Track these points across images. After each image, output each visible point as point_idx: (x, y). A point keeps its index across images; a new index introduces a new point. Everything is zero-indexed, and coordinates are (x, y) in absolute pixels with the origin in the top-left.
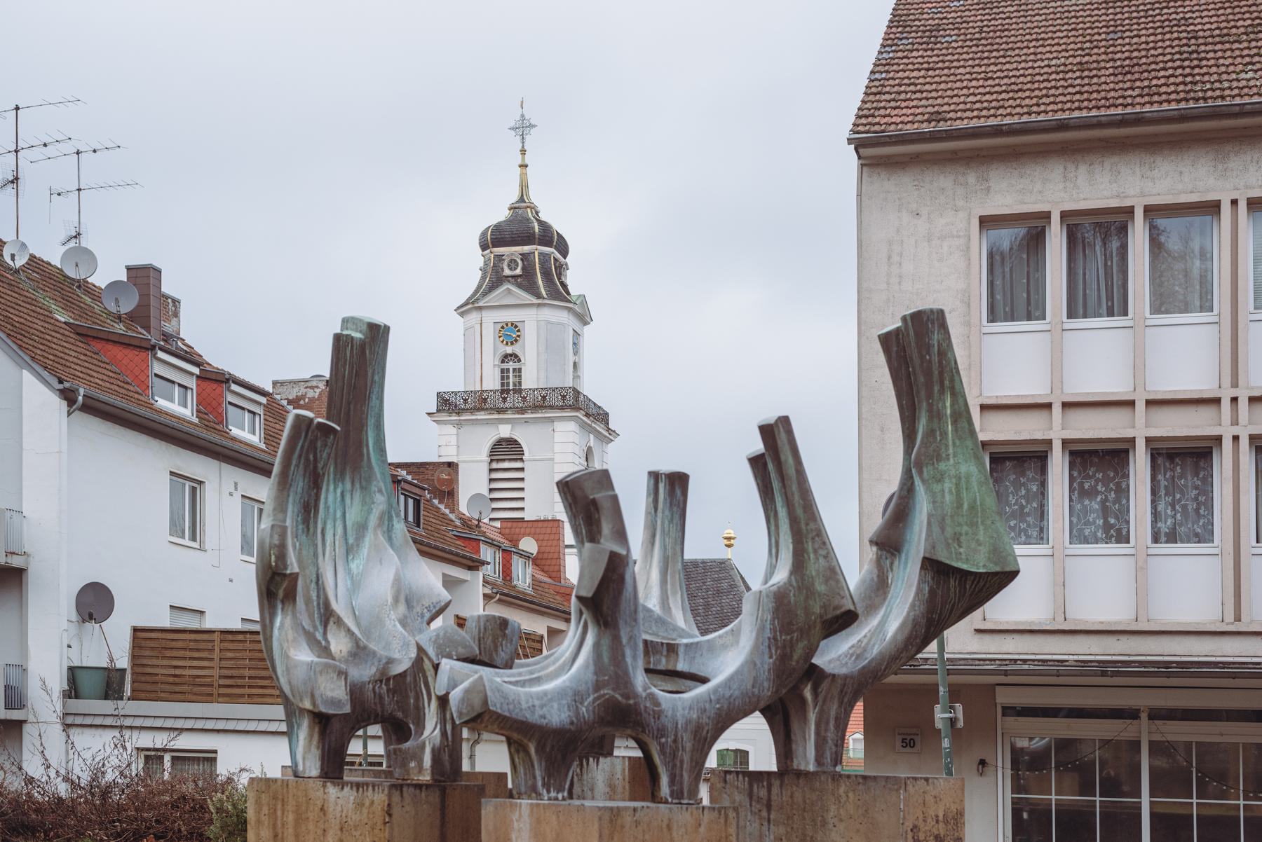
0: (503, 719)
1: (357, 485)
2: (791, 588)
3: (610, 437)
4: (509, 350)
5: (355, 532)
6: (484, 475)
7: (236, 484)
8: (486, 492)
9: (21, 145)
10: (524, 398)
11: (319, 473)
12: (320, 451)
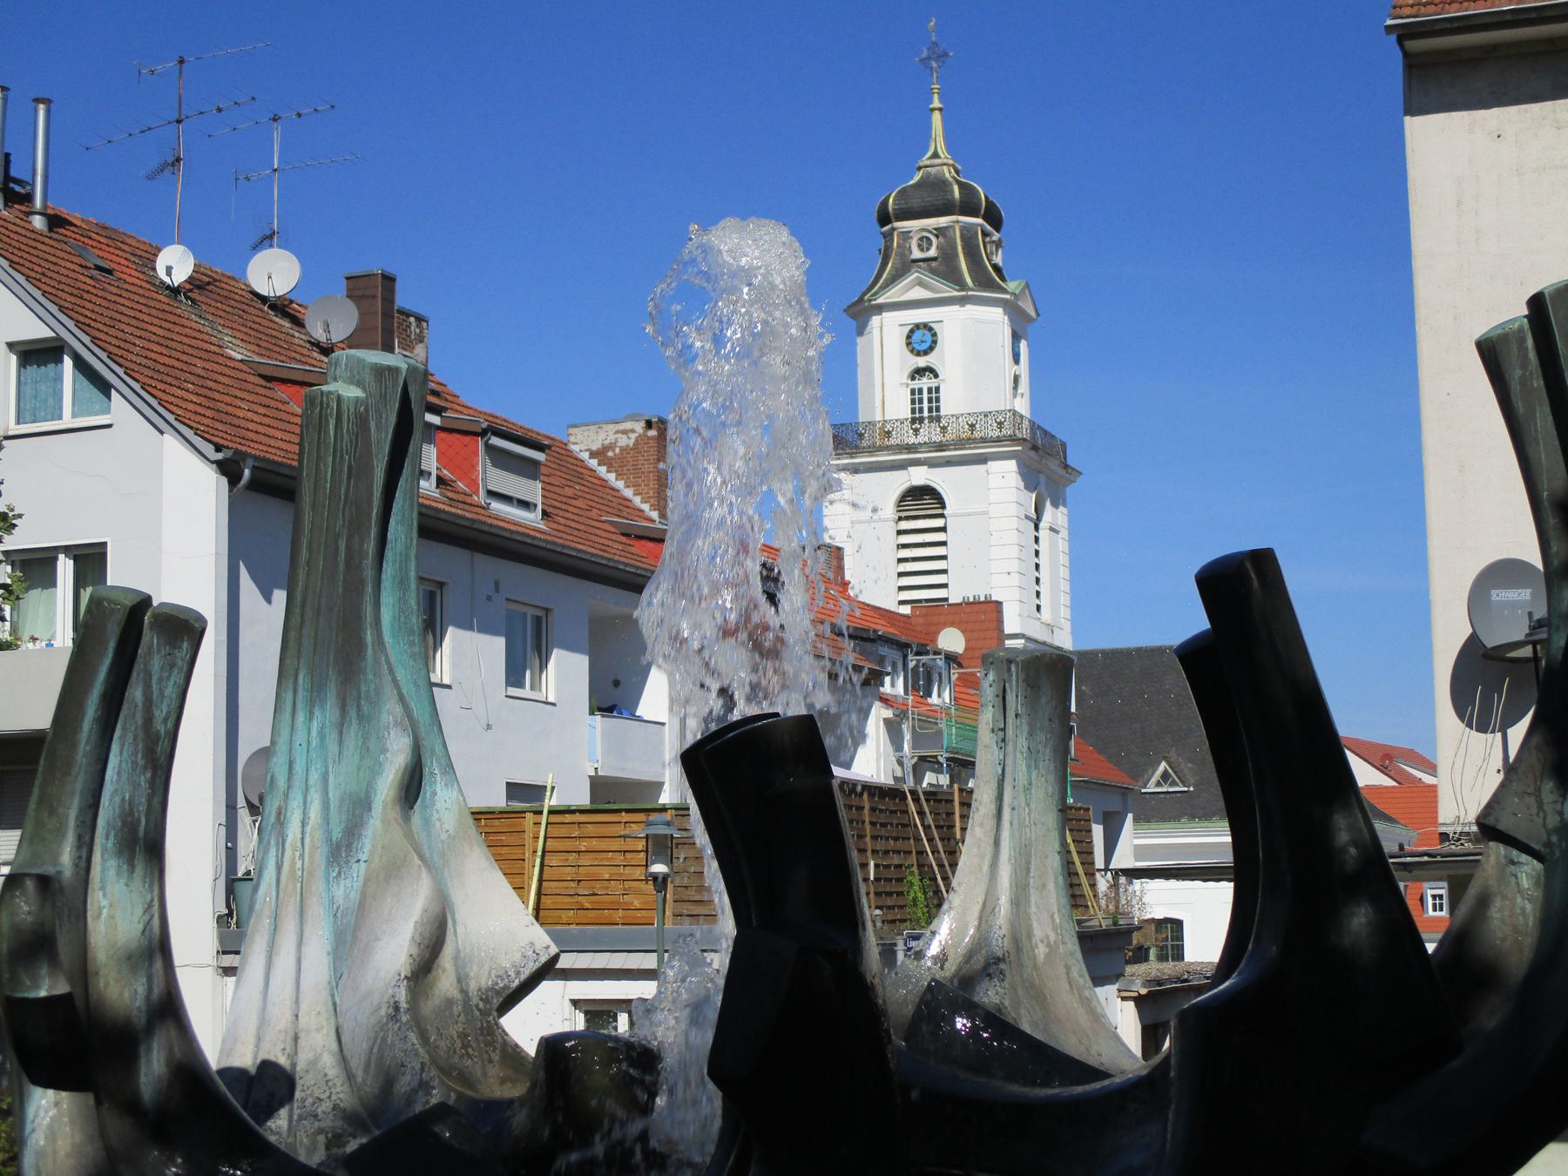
1: (353, 713)
4: (922, 362)
7: (497, 584)
9: (184, 113)
10: (944, 429)
11: (158, 734)
12: (160, 680)
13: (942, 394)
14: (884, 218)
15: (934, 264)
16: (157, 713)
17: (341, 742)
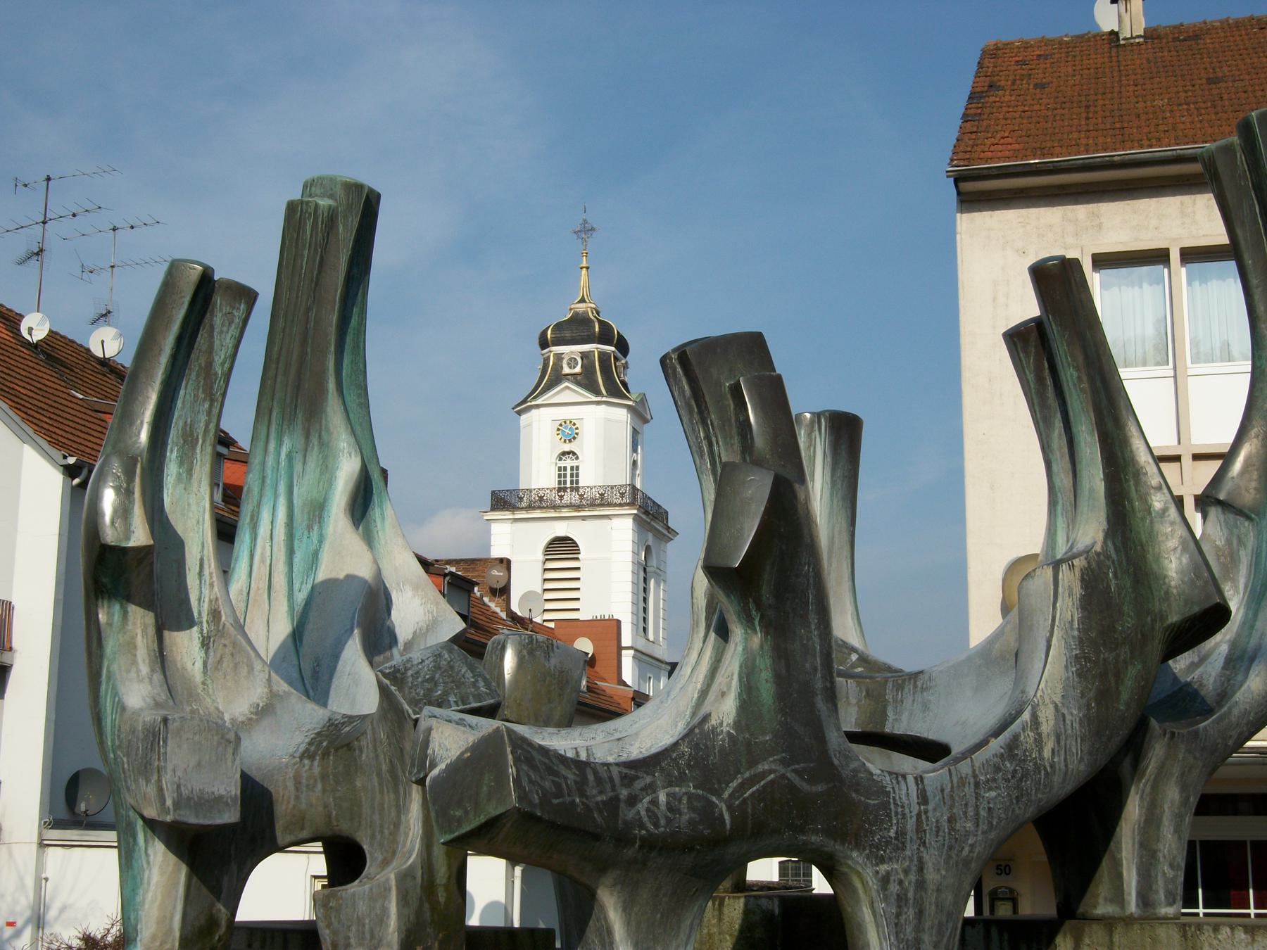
0: (808, 881)
1: (315, 441)
2: (1109, 563)
3: (669, 535)
4: (567, 448)
5: (306, 517)
6: (538, 575)
8: (540, 591)
9: (49, 215)
13: (580, 472)
14: (544, 344)
15: (579, 378)
16: (216, 358)
17: (305, 462)
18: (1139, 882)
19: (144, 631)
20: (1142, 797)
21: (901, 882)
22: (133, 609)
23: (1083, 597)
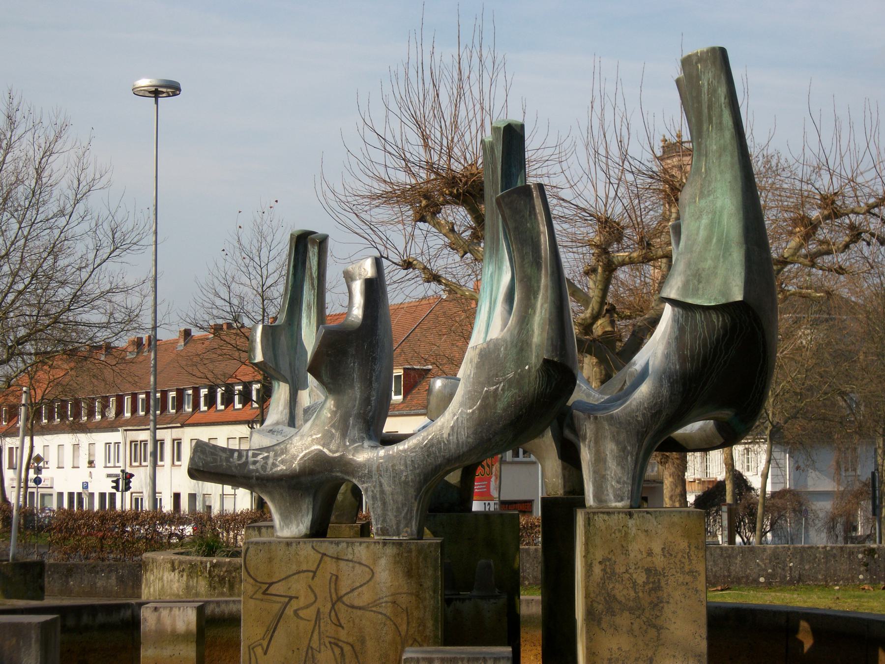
18: (594, 490)
19: (285, 393)
20: (589, 449)
21: (373, 491)
22: (281, 383)
23: (478, 363)
